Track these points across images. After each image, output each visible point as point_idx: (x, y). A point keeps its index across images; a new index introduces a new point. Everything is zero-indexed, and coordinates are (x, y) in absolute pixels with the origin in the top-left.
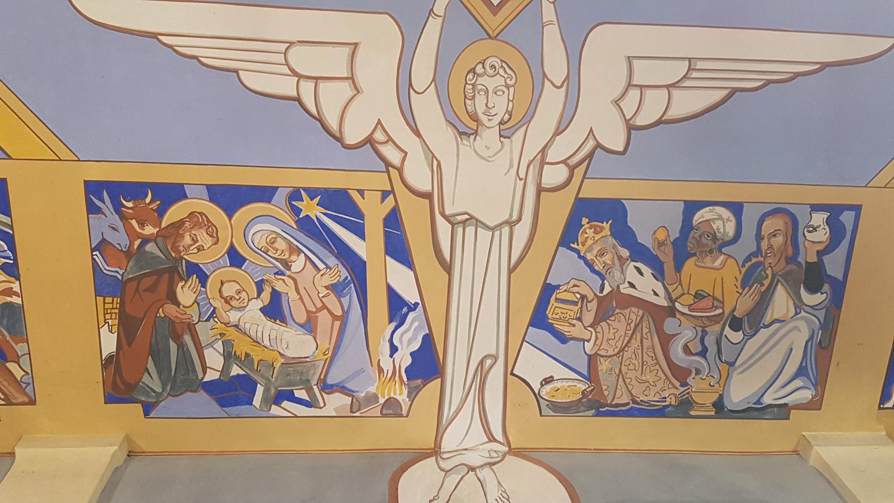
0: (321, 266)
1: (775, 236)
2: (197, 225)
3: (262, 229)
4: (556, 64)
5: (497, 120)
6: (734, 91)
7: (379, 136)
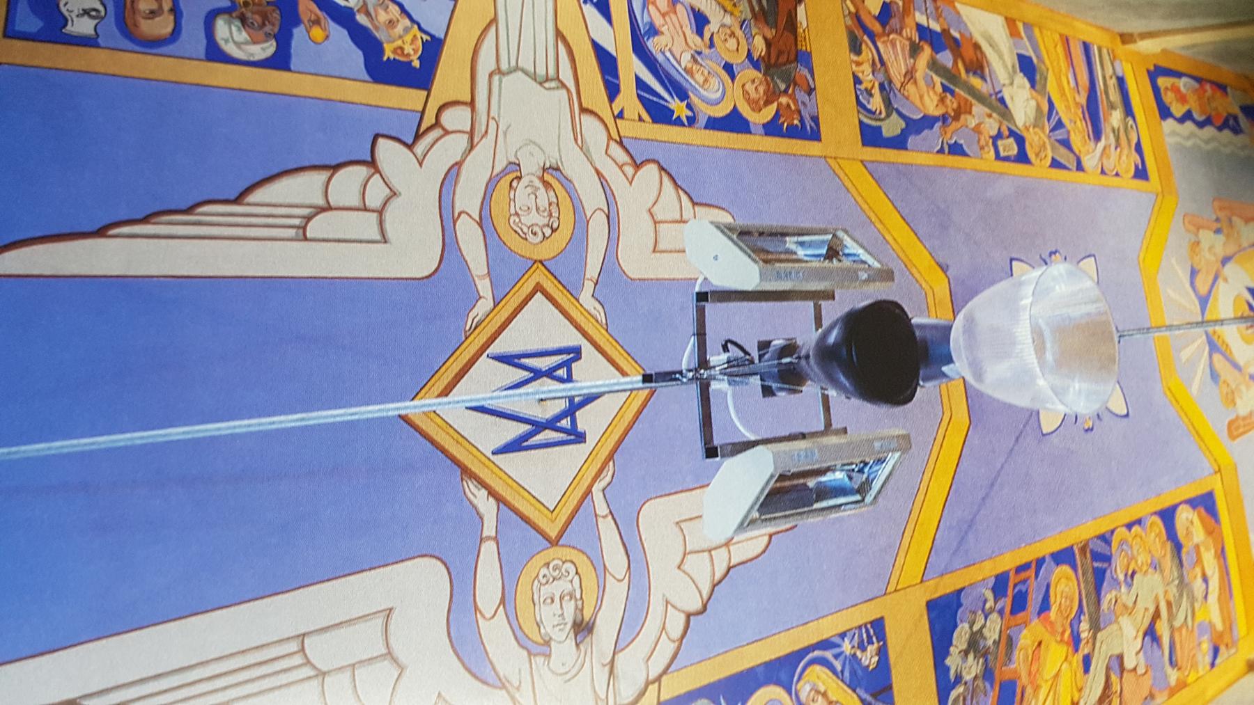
0: (668, 54)
1: (152, 12)
2: (757, 102)
3: (713, 93)
4: (469, 237)
5: (524, 181)
6: (237, 200)
7: (629, 170)
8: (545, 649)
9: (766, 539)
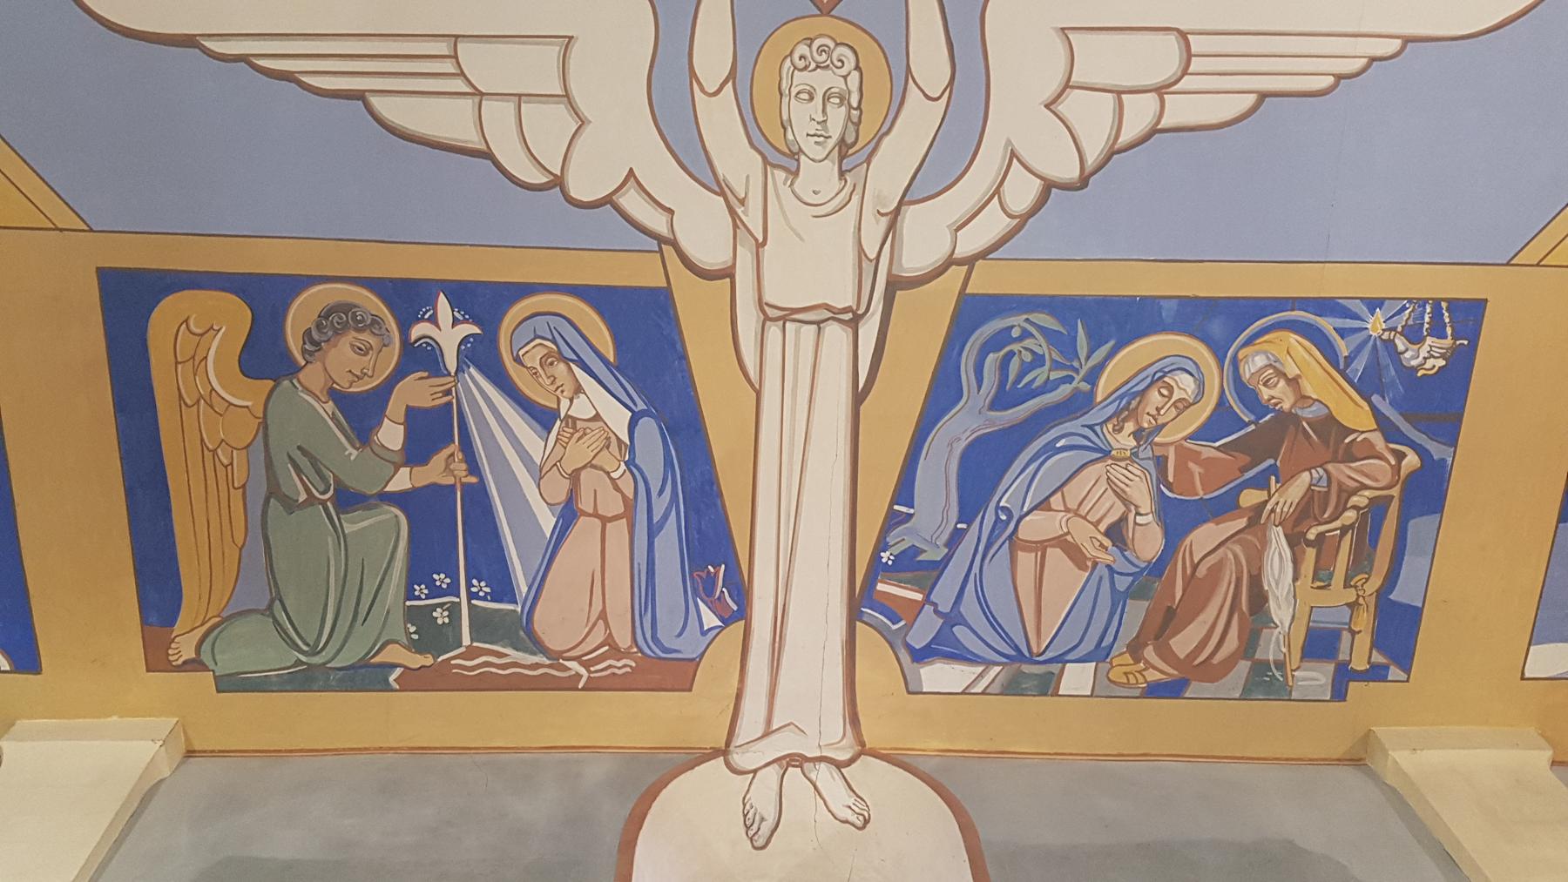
8: (792, 165)
9: (1252, 98)
